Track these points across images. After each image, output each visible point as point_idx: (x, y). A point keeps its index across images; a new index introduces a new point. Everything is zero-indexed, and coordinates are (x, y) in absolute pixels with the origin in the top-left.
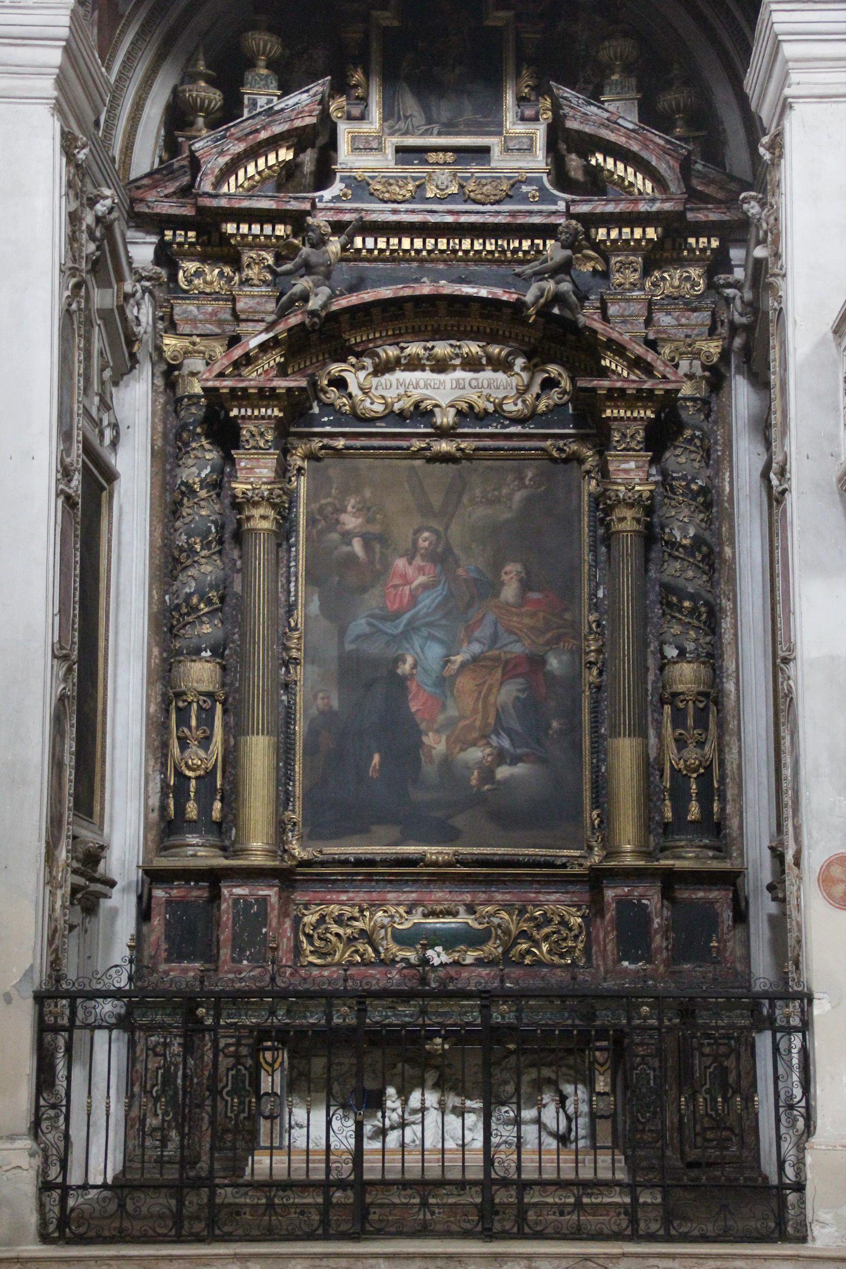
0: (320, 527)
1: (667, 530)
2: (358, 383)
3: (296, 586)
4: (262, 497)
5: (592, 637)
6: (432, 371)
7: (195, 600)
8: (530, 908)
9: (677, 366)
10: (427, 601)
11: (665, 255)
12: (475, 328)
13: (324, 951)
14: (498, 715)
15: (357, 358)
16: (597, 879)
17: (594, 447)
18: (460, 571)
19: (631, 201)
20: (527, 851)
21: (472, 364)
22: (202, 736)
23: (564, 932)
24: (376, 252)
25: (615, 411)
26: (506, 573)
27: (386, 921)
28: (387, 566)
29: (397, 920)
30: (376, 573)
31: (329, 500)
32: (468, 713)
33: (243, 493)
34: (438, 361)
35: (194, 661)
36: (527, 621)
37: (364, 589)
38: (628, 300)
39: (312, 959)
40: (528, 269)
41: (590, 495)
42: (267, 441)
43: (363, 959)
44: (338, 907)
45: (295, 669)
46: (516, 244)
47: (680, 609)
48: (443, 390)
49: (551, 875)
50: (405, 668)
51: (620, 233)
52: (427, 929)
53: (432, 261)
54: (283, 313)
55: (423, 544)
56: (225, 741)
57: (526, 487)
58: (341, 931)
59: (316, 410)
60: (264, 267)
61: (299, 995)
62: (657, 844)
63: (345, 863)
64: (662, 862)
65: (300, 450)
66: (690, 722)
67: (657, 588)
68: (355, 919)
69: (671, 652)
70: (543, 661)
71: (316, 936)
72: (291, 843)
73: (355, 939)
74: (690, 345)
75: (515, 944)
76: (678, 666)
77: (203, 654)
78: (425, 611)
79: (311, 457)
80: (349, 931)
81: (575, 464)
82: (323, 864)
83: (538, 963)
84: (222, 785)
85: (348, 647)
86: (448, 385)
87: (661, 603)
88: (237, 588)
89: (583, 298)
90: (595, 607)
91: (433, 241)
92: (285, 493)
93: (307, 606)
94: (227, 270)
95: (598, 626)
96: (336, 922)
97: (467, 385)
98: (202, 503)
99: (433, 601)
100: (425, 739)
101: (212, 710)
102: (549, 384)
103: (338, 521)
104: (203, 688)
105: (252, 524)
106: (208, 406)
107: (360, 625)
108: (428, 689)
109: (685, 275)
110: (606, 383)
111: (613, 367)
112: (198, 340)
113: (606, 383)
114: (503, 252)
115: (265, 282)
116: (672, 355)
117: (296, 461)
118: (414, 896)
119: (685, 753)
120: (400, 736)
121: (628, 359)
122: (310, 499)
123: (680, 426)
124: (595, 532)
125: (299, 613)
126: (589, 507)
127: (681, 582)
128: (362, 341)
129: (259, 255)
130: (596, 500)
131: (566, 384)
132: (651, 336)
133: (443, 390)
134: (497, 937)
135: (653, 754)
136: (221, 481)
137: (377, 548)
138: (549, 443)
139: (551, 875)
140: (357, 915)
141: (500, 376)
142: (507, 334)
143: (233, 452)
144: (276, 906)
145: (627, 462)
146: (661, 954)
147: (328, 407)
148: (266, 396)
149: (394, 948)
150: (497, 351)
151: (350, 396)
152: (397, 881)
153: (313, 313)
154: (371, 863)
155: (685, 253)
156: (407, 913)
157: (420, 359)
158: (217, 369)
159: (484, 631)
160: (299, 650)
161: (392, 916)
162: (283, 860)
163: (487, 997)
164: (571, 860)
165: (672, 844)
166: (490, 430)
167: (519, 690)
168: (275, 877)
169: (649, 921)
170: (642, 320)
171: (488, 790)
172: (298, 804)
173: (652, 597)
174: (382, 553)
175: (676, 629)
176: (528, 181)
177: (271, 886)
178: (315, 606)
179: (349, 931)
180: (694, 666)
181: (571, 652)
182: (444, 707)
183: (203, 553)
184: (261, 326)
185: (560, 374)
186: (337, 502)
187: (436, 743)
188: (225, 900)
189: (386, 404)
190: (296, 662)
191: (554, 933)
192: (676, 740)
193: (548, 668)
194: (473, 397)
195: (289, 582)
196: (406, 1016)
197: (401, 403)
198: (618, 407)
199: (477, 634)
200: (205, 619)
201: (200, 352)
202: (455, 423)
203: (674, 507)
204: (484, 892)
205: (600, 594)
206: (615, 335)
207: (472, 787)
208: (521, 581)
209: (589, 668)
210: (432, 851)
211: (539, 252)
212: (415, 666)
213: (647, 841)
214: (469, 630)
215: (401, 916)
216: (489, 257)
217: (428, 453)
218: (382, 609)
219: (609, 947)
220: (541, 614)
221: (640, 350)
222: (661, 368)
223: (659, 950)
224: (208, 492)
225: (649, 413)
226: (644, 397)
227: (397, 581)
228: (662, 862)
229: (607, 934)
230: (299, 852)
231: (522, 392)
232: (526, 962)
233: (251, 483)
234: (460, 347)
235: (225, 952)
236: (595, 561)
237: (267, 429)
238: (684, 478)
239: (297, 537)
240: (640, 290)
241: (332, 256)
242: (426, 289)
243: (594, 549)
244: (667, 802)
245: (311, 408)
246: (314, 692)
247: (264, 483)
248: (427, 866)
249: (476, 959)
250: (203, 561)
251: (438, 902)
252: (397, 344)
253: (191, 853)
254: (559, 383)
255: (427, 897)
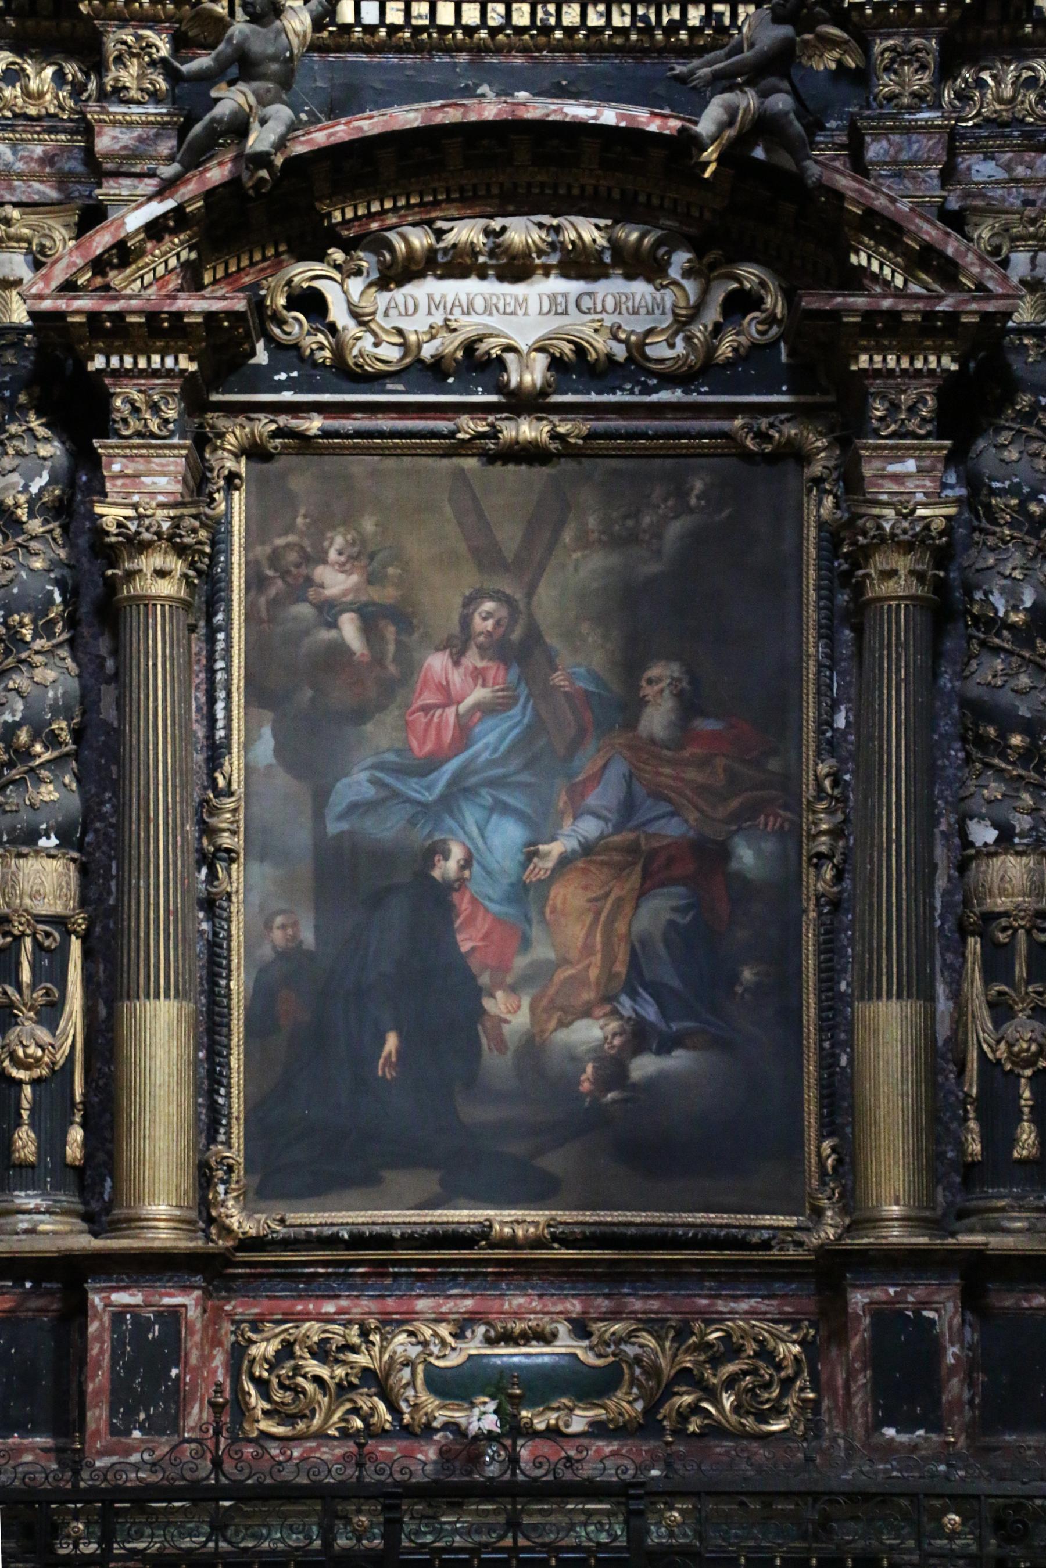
0: (273, 592)
1: (978, 595)
2: (349, 303)
3: (228, 709)
4: (158, 534)
5: (821, 806)
6: (501, 278)
7: (23, 736)
8: (698, 1326)
9: (1005, 263)
10: (491, 738)
11: (986, 32)
12: (589, 190)
13: (292, 1410)
14: (633, 953)
15: (347, 252)
16: (831, 1273)
17: (831, 430)
18: (558, 679)
20: (689, 1218)
21: (579, 264)
22: (42, 1001)
23: (766, 1372)
24: (383, 32)
25: (878, 358)
26: (650, 682)
27: (414, 1352)
28: (409, 667)
29: (435, 1350)
30: (387, 684)
31: (292, 538)
32: (574, 954)
33: (120, 525)
34: (513, 258)
35: (24, 856)
36: (692, 774)
37: (360, 715)
38: (909, 130)
39: (265, 1425)
40: (703, 69)
41: (821, 525)
42: (166, 421)
43: (367, 1425)
44: (317, 1326)
45: (229, 871)
46: (676, 13)
47: (1002, 749)
48: (525, 318)
49: (745, 1266)
50: (449, 867)
52: (495, 1366)
53: (498, 50)
54: (195, 158)
55: (482, 625)
56: (89, 1012)
57: (691, 511)
58: (324, 1372)
59: (262, 357)
60: (153, 63)
61: (239, 1492)
62: (950, 1204)
63: (332, 1242)
64: (965, 1239)
65: (230, 438)
66: (1020, 969)
67: (955, 710)
68: (354, 1349)
69: (984, 834)
70: (723, 853)
71: (275, 1381)
72: (223, 1203)
73: (352, 1387)
74: (1033, 222)
75: (669, 1393)
76: (997, 862)
77: (43, 842)
78: (486, 755)
79: (254, 452)
80: (340, 1371)
81: (791, 465)
82: (286, 1244)
83: (715, 1430)
84: (84, 1095)
85: (333, 828)
86: (533, 307)
87: (964, 740)
88: (108, 712)
89: (814, 126)
90: (829, 746)
91: (501, 8)
92: (203, 525)
93: (250, 749)
94: (71, 69)
95: (835, 784)
96: (314, 1355)
97: (572, 308)
98: (34, 545)
99: (502, 739)
100: (488, 1004)
101: (64, 950)
102: (740, 304)
103: (309, 581)
104: (44, 908)
105: (138, 587)
106: (40, 349)
107: (356, 784)
108: (494, 908)
109: (1026, 74)
110: (860, 302)
111: (875, 267)
112: (15, 214)
113: (860, 302)
114: (648, 30)
115: (155, 96)
116: (996, 241)
117: (226, 461)
118: (468, 1303)
119: (1010, 1029)
120: (442, 1000)
121: (905, 251)
122: (255, 534)
123: (1010, 386)
124: (831, 599)
125: (234, 765)
126: (819, 548)
127: (1007, 697)
128: (356, 218)
129: (139, 38)
130: (832, 536)
131: (774, 302)
132: (954, 204)
133: (525, 318)
134: (634, 1381)
135: (943, 1031)
136: (71, 499)
137: (390, 631)
138: (738, 422)
139: (745, 1266)
140: (356, 1340)
141: (641, 289)
142: (655, 201)
143: (96, 443)
144: (198, 1326)
145: (900, 460)
146: (961, 1412)
147: (287, 353)
148: (162, 330)
149: (430, 1402)
150: (634, 236)
151: (332, 329)
152: (437, 1278)
153: (262, 159)
154: (383, 1241)
155: (1028, 28)
156: (454, 1336)
157: (475, 254)
158: (59, 274)
159: (605, 795)
160: (234, 833)
161: (425, 1344)
162: (208, 1238)
163: (630, 1497)
164: (780, 1235)
165: (981, 1203)
166: (618, 397)
167: (675, 909)
168: (195, 1272)
169: (939, 1352)
170: (934, 170)
171: (614, 1102)
172: (238, 1131)
173: (945, 726)
174: (398, 643)
175: (995, 790)
177: (186, 1289)
178: (266, 747)
179: (340, 1371)
180: (1029, 861)
181: (781, 834)
182: (526, 943)
183: (39, 644)
184: (149, 186)
185: (763, 284)
186: (306, 543)
187: (511, 1013)
188: (96, 1315)
189: (405, 345)
190: (230, 856)
191: (745, 1373)
192: (992, 1005)
193: (734, 865)
194: (583, 327)
195: (212, 701)
196: (456, 1531)
197: (437, 342)
198: (884, 351)
199: (592, 801)
200: (44, 773)
201: (19, 239)
202: (547, 384)
203: (992, 549)
204: (607, 1296)
205: (840, 722)
206: (880, 202)
207: (581, 1096)
208: (679, 695)
209: (817, 867)
210: (504, 1219)
211: (722, 30)
212: (467, 863)
213: (932, 1198)
214: (577, 793)
215: (444, 1343)
216: (618, 41)
217: (491, 445)
218: (398, 752)
219: (857, 1401)
220: (720, 762)
221: (931, 232)
222: (975, 270)
223: (957, 1404)
224: (46, 522)
225: (946, 361)
226: (937, 329)
227: (429, 698)
228: (965, 1239)
229: (851, 1376)
230: (239, 1220)
231: (682, 322)
232: (692, 1428)
233: (135, 506)
234: (557, 229)
235: (97, 1416)
236: (830, 657)
237: (165, 396)
238: (1014, 490)
239: (229, 611)
240: (931, 108)
241: (295, 42)
242: (489, 108)
243: (828, 634)
244: (972, 1124)
245: (253, 353)
246: (262, 913)
247: (162, 506)
248: (492, 1246)
249: (591, 1424)
250: (38, 659)
251: (517, 1315)
252: (429, 223)
253: (25, 1226)
254: (761, 300)
255: (495, 1305)
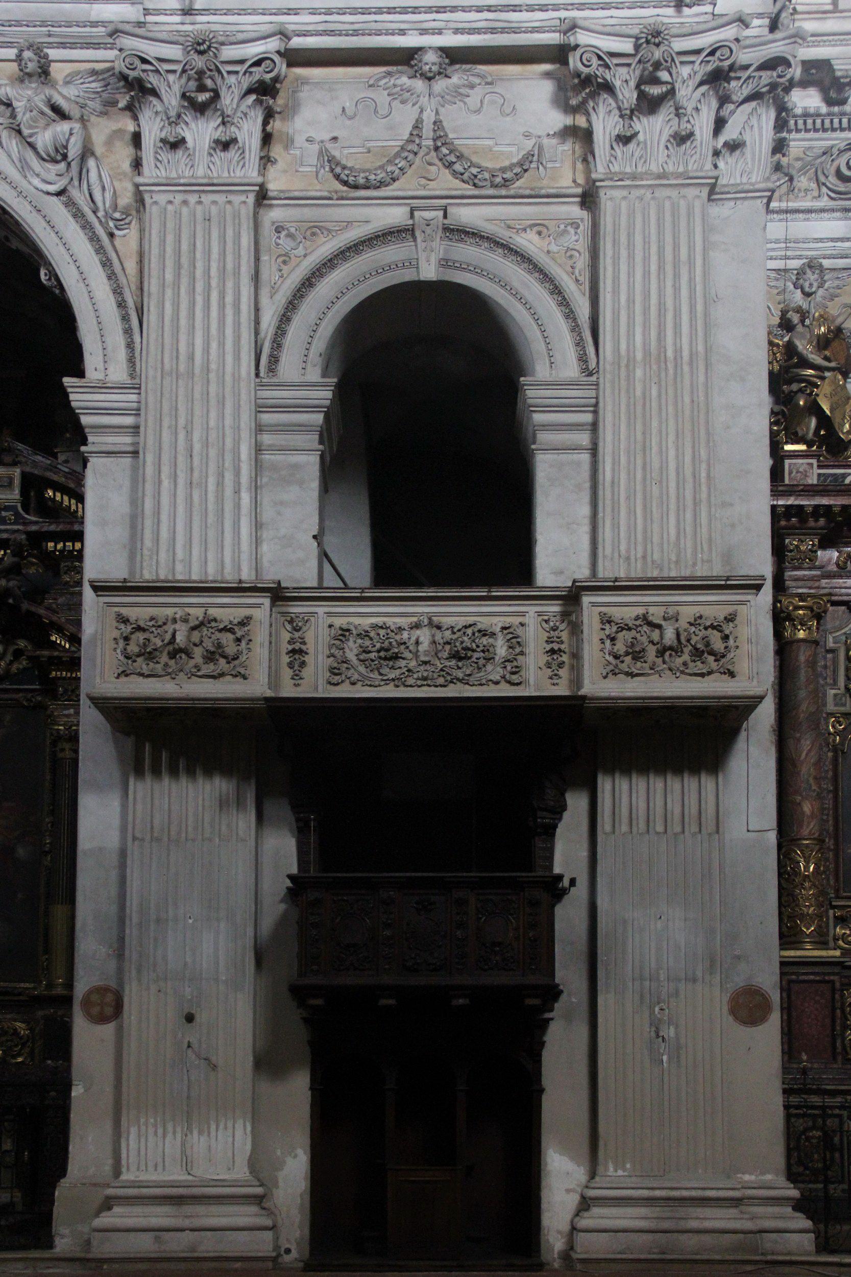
19: (69, 523)
51: (65, 545)
102: (18, 654)
113: (46, 653)
138: (21, 695)
145: (69, 709)
176: (6, 508)
198: (61, 671)
